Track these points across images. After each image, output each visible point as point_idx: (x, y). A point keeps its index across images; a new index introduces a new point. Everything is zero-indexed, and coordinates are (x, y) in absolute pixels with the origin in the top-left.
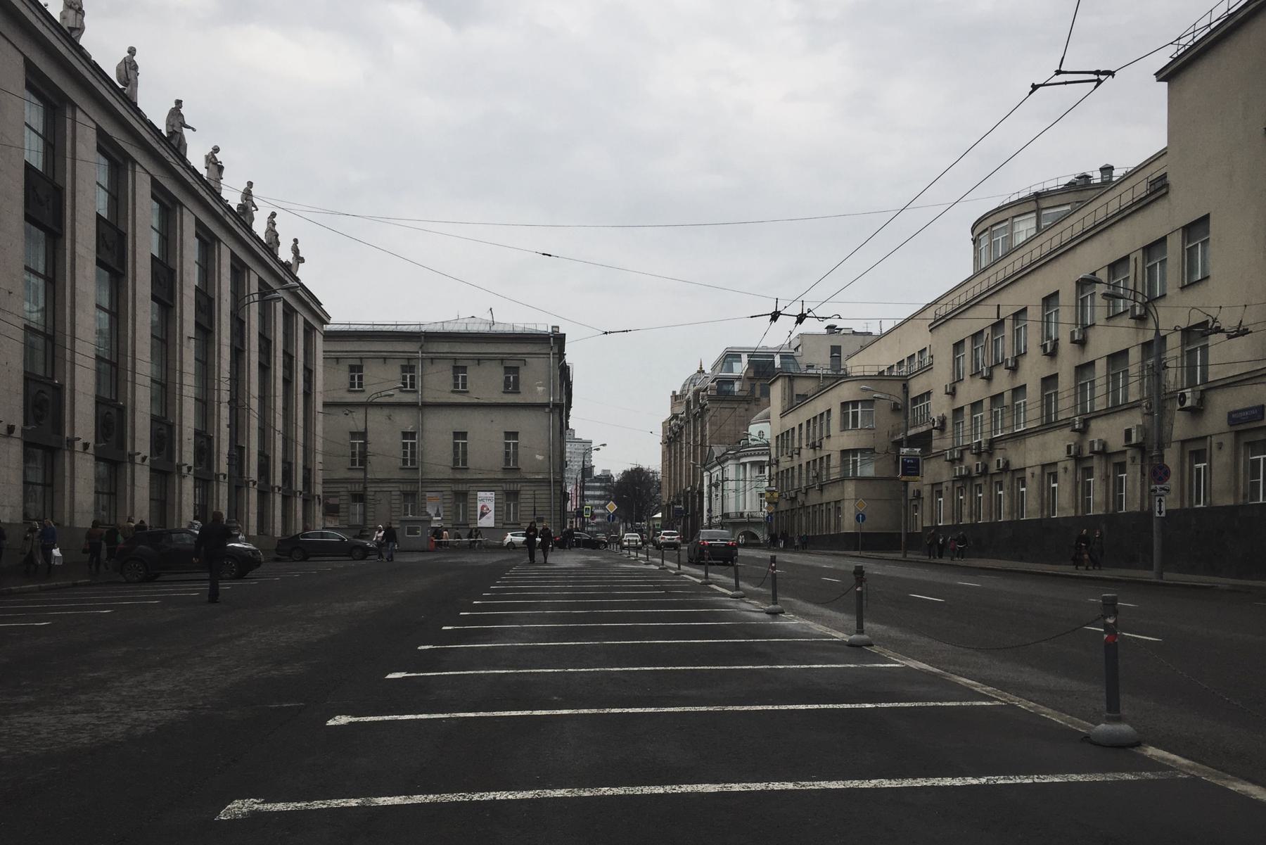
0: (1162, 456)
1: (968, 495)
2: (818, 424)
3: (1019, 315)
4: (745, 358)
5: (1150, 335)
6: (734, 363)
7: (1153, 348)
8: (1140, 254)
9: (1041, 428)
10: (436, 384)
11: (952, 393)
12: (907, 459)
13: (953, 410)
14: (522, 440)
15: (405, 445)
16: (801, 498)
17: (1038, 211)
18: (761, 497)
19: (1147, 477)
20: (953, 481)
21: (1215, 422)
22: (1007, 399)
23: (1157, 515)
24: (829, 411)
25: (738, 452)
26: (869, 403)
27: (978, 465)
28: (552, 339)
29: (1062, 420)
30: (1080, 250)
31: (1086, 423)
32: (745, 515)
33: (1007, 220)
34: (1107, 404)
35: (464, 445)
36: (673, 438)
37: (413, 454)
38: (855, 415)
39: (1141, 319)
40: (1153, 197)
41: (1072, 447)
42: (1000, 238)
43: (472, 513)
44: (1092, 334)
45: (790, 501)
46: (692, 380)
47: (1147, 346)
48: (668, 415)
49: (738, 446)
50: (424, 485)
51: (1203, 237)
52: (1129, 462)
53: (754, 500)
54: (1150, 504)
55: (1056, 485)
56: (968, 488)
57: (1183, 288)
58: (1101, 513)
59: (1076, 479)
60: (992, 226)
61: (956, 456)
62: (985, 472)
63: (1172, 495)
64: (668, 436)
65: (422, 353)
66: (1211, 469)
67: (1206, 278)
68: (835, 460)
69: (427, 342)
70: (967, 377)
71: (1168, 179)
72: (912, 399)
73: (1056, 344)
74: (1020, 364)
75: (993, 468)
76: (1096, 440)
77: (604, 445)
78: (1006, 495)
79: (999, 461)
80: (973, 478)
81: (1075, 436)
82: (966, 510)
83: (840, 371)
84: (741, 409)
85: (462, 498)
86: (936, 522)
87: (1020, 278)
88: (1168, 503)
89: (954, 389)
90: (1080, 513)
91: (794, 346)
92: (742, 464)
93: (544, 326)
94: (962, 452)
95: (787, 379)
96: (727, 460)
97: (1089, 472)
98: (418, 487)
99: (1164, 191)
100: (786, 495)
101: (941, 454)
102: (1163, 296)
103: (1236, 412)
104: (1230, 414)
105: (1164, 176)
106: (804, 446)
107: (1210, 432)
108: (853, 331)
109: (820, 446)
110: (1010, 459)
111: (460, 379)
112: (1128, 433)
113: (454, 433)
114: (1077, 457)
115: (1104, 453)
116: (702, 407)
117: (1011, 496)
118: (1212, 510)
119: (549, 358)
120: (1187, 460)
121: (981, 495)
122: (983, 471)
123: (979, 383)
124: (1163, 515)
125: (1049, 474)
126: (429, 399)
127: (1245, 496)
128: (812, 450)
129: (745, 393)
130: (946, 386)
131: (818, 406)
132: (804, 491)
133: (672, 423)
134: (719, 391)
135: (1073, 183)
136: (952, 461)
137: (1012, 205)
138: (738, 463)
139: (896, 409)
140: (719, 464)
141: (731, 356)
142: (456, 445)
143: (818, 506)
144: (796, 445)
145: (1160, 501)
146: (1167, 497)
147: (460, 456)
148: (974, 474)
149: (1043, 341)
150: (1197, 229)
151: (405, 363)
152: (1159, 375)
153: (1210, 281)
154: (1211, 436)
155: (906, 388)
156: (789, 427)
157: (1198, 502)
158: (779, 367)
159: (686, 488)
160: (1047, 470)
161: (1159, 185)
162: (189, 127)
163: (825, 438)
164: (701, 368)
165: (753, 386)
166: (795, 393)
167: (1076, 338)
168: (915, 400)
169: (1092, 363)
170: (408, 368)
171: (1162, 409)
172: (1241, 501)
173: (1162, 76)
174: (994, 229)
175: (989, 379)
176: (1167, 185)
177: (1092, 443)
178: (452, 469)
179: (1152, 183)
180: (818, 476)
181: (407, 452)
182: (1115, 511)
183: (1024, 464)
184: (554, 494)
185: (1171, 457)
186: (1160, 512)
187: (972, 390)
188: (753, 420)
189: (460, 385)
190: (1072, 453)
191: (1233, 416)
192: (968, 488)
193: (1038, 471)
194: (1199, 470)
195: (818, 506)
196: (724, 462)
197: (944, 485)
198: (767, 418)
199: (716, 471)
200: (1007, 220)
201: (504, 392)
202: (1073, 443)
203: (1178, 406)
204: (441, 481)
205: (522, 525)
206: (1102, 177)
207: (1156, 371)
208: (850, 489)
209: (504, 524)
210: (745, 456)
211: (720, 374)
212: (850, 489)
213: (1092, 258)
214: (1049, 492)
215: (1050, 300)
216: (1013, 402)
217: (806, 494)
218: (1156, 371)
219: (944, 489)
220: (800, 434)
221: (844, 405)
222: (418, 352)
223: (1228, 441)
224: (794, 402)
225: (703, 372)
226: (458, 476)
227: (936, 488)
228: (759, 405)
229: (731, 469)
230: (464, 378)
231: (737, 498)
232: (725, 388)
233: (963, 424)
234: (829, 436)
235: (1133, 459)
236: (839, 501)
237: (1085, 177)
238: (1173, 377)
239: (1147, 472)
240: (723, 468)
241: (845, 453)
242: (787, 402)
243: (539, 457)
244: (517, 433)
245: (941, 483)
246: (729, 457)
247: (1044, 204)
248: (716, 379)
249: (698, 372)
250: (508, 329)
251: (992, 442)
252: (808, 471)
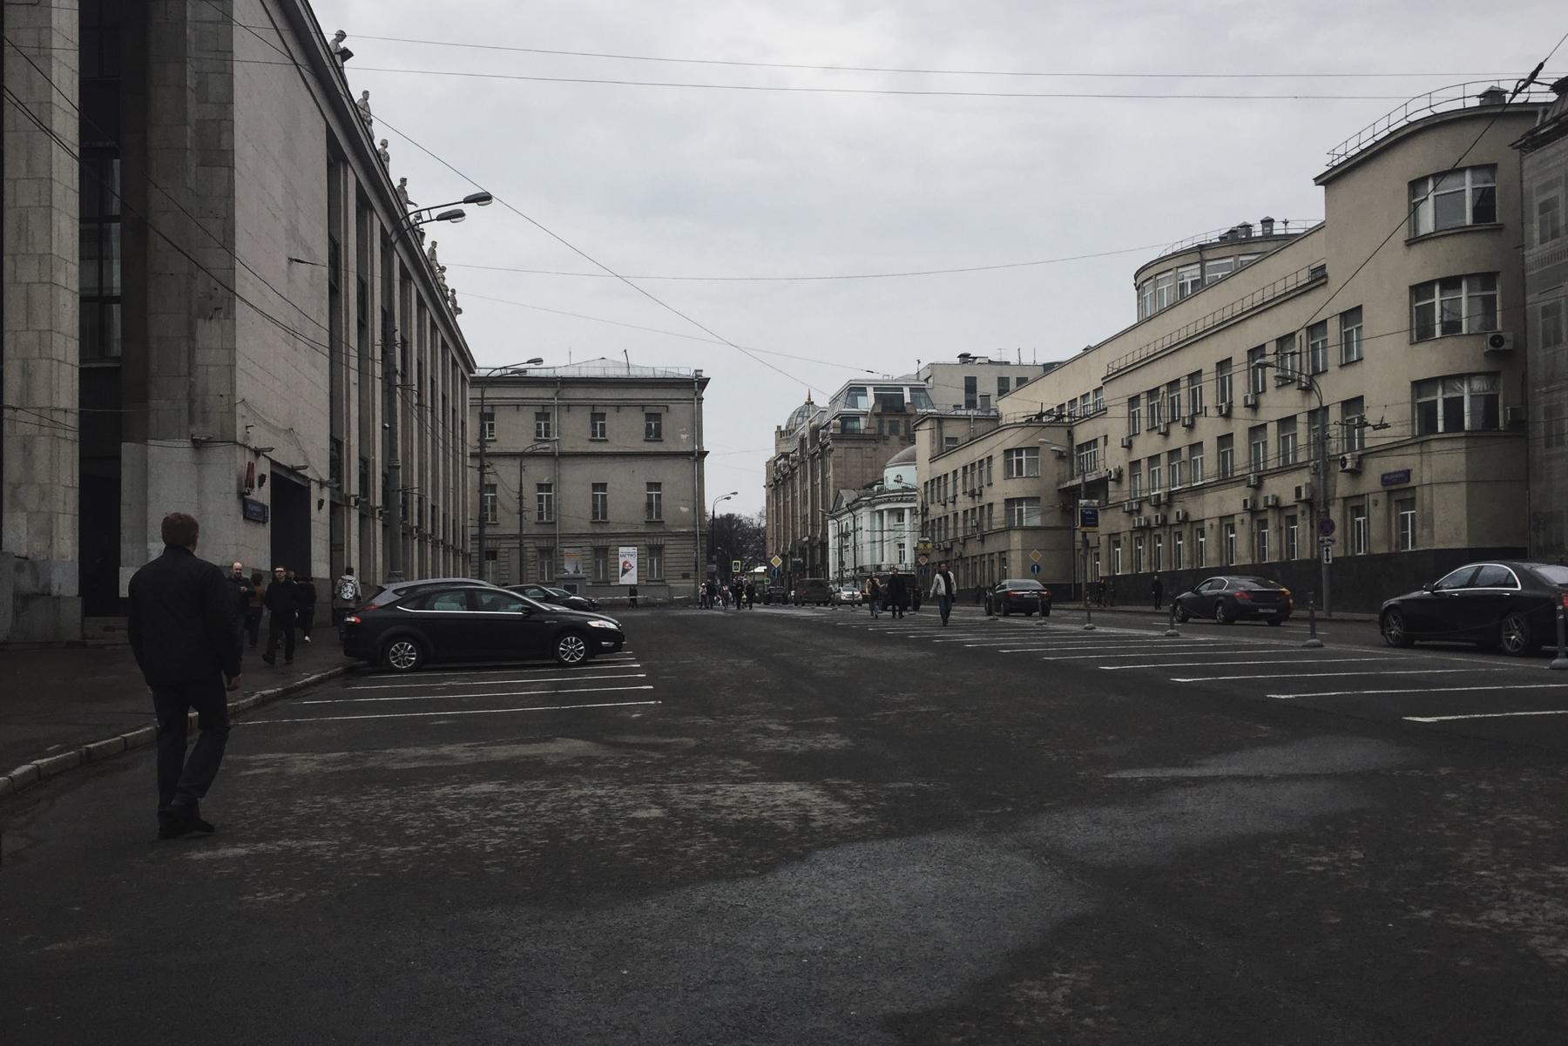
0: (1327, 513)
1: (1147, 545)
2: (977, 471)
3: (1195, 376)
4: (870, 391)
5: (1315, 404)
6: (859, 397)
7: (1318, 415)
8: (1303, 333)
9: (1218, 483)
10: (573, 431)
11: (1129, 446)
12: (1087, 510)
13: (1130, 463)
14: (666, 491)
15: (540, 498)
16: (957, 549)
17: (1202, 262)
18: (900, 547)
19: (1315, 529)
20: (1132, 532)
21: (1371, 481)
22: (1185, 454)
23: (1326, 562)
24: (990, 458)
25: (874, 498)
26: (1034, 450)
27: (1157, 517)
28: (696, 384)
29: (1238, 476)
30: (1250, 323)
31: (1260, 479)
32: (884, 568)
33: (1171, 270)
34: (1279, 464)
35: (604, 497)
36: (780, 480)
37: (549, 505)
38: (1020, 462)
39: (1308, 390)
40: (1313, 285)
41: (1249, 502)
42: (1165, 287)
43: (613, 570)
44: (1263, 400)
45: (943, 553)
46: (800, 413)
47: (1312, 414)
48: (772, 454)
49: (870, 490)
50: (562, 540)
51: (1357, 323)
52: (1299, 515)
53: (892, 551)
54: (1319, 552)
55: (1233, 536)
56: (1147, 539)
57: (1341, 366)
58: (1276, 561)
59: (1252, 529)
60: (1156, 275)
61: (1134, 508)
62: (1164, 523)
63: (1337, 544)
64: (774, 478)
65: (558, 399)
66: (1369, 522)
67: (1360, 359)
68: (999, 511)
69: (563, 388)
70: (1143, 431)
71: (1327, 270)
72: (1077, 446)
73: (1230, 407)
74: (1196, 423)
75: (1172, 519)
76: (1270, 495)
77: (735, 493)
78: (1186, 545)
79: (1178, 513)
80: (1151, 529)
81: (1250, 491)
82: (1144, 560)
83: (989, 412)
84: (868, 449)
85: (603, 554)
86: (1114, 571)
87: (1194, 342)
88: (1335, 551)
89: (1130, 442)
90: (1256, 562)
91: (922, 377)
92: (878, 511)
93: (686, 372)
94: (1140, 503)
95: (936, 421)
96: (861, 507)
97: (1263, 524)
98: (556, 544)
99: (1323, 281)
100: (940, 546)
101: (1119, 505)
102: (1325, 371)
103: (1389, 474)
104: (1383, 476)
105: (1323, 267)
106: (960, 491)
107: (1368, 491)
108: (989, 361)
109: (980, 495)
110: (1188, 511)
111: (598, 426)
112: (1298, 490)
113: (593, 484)
114: (1253, 510)
115: (1277, 507)
116: (823, 447)
117: (1191, 545)
118: (1371, 558)
119: (694, 404)
120: (1349, 513)
121: (1160, 545)
122: (1162, 521)
123: (1156, 439)
124: (1330, 562)
125: (1227, 525)
126: (566, 448)
127: (1397, 546)
128: (970, 498)
129: (872, 432)
130: (1123, 440)
131: (977, 452)
132: (961, 541)
133: (779, 463)
134: (843, 427)
135: (1235, 231)
136: (1131, 513)
137: (1175, 255)
138: (872, 510)
139: (1060, 456)
140: (850, 511)
141: (855, 390)
142: (595, 497)
143: (978, 558)
144: (950, 494)
145: (1327, 550)
146: (1333, 546)
147: (599, 511)
148: (1153, 524)
149: (1217, 402)
150: (1352, 316)
151: (539, 410)
152: (1323, 444)
153: (1364, 362)
154: (1368, 494)
155: (1070, 434)
156: (941, 472)
157: (1360, 550)
158: (909, 401)
159: (801, 538)
160: (1225, 522)
161: (1319, 274)
162: (412, 203)
163: (985, 486)
164: (809, 399)
165: (881, 423)
166: (944, 437)
167: (1249, 403)
168: (1081, 447)
169: (1264, 426)
170: (543, 415)
171: (1327, 470)
172: (1394, 549)
173: (1320, 181)
174: (1159, 277)
175: (1166, 434)
176: (1326, 276)
177: (1266, 498)
178: (592, 522)
179: (1314, 271)
180: (978, 526)
181: (542, 505)
182: (1288, 559)
183: (1203, 515)
184: (701, 548)
185: (1335, 514)
186: (1328, 560)
187: (1148, 444)
188: (888, 464)
189: (599, 433)
190: (1249, 507)
191: (1386, 478)
192: (1147, 539)
193: (1216, 522)
194: (1359, 523)
195: (978, 558)
196: (856, 509)
197: (1122, 535)
198: (911, 459)
199: (847, 520)
200: (1171, 270)
201: (645, 440)
202: (1248, 498)
203: (1340, 468)
204: (579, 536)
205: (667, 581)
206: (1263, 230)
207: (1321, 441)
208: (1016, 539)
209: (647, 581)
210: (881, 503)
211: (844, 410)
212: (1016, 539)
213: (1264, 330)
214: (1227, 542)
215: (1224, 365)
216: (1190, 459)
217: (964, 544)
218: (1321, 441)
219: (1122, 539)
220: (955, 481)
221: (1008, 452)
222: (554, 399)
223: (1382, 498)
224: (945, 447)
225: (812, 403)
226: (598, 531)
227: (1114, 540)
228: (887, 444)
229: (865, 518)
230: (603, 426)
231: (873, 549)
232: (849, 425)
233: (1140, 477)
234: (990, 484)
235: (1303, 513)
236: (1004, 552)
237: (1247, 227)
238: (1335, 447)
239: (1315, 525)
240: (854, 516)
241: (1009, 502)
242: (936, 446)
243: (684, 510)
244: (660, 483)
245: (1119, 534)
246: (864, 503)
247: (1208, 255)
248: (839, 415)
249: (806, 403)
250: (649, 374)
251: (1170, 495)
252: (965, 521)
